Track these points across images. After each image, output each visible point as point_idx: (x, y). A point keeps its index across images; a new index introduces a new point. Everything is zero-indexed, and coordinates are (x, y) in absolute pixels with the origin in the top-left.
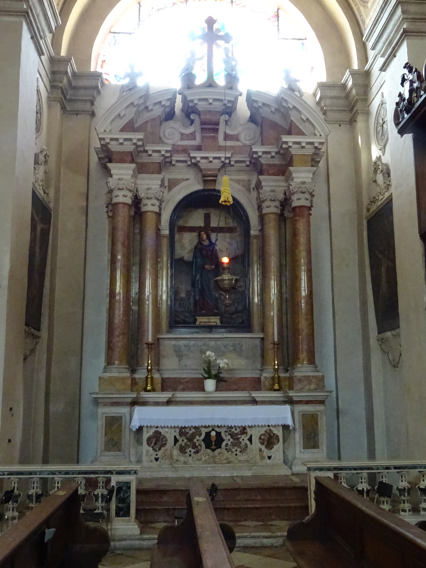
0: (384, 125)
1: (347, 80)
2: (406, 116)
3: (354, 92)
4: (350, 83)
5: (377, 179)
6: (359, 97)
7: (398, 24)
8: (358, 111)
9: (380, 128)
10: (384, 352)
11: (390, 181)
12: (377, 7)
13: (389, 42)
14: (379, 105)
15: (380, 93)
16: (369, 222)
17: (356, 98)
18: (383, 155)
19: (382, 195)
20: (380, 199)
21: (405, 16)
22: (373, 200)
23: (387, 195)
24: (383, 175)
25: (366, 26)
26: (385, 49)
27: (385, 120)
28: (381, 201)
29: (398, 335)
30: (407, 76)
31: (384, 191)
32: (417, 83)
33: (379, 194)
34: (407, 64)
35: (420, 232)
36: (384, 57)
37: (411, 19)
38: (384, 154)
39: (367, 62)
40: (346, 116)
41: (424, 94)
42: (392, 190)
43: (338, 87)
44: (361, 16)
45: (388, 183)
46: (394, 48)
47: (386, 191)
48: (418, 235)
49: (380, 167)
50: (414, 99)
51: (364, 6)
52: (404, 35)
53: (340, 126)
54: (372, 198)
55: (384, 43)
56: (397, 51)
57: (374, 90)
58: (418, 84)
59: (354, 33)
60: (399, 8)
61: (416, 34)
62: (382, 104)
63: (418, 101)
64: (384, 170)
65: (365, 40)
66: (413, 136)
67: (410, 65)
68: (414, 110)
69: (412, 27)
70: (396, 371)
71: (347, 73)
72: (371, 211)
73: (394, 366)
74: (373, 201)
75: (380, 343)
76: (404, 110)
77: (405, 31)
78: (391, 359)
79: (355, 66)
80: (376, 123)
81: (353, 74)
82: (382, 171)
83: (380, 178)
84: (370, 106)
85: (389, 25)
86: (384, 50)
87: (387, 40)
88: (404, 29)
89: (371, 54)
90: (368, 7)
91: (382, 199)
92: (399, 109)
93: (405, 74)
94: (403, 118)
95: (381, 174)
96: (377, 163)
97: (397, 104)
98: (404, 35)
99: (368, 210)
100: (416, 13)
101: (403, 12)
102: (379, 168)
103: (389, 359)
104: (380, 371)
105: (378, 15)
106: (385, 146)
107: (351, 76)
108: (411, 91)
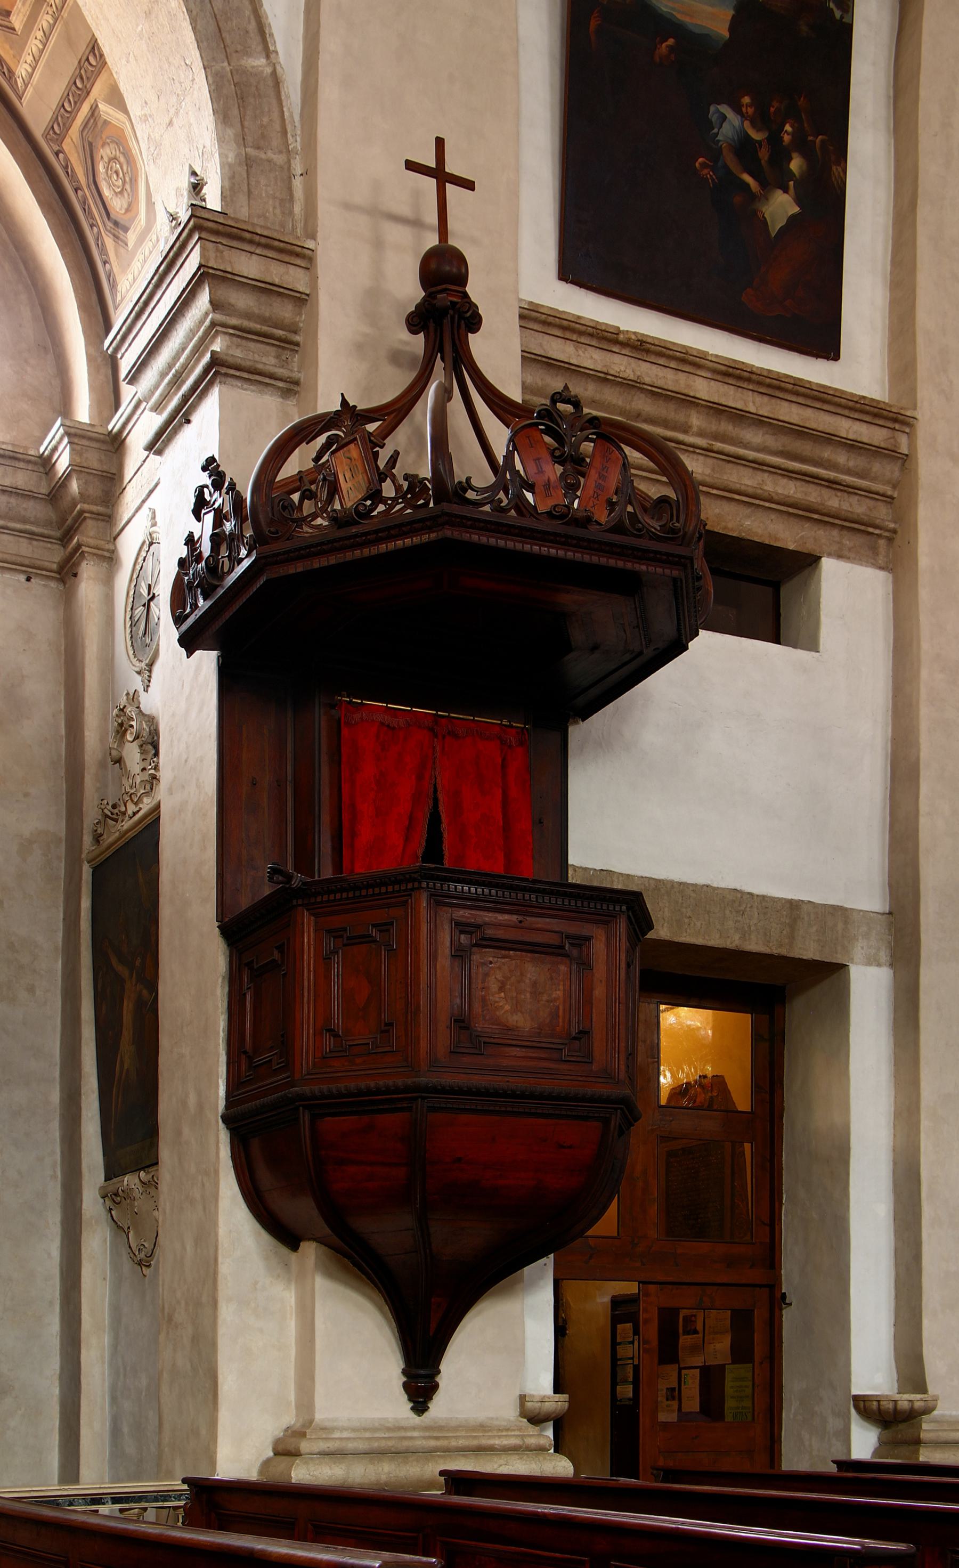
0: (152, 603)
1: (55, 449)
2: (201, 602)
3: (74, 486)
4: (63, 463)
5: (124, 754)
6: (86, 507)
7: (200, 333)
8: (84, 548)
9: (140, 610)
10: (119, 1227)
11: (156, 768)
12: (151, 252)
13: (174, 376)
14: (144, 543)
15: (145, 512)
16: (96, 871)
17: (79, 507)
18: (146, 690)
19: (136, 804)
20: (130, 812)
21: (219, 317)
22: (112, 814)
23: (147, 804)
24: (141, 746)
25: (119, 298)
26: (164, 390)
27: (156, 591)
28: (131, 818)
29: (151, 1185)
30: (211, 495)
31: (142, 791)
32: (233, 523)
33: (127, 798)
34: (211, 460)
35: (220, 916)
36: (160, 413)
37: (234, 328)
38: (148, 686)
39: (117, 405)
40: (53, 555)
41: (246, 557)
42: (162, 792)
43: (29, 462)
44: (105, 263)
45: (152, 772)
46: (185, 398)
47: (147, 794)
48: (217, 924)
49: (134, 723)
50: (223, 562)
51: (116, 237)
52: (214, 370)
53: (28, 579)
54: (109, 807)
55: (163, 375)
56: (194, 407)
57: (131, 497)
58: (235, 526)
59: (83, 307)
60: (204, 289)
61: (245, 375)
62: (151, 544)
63: (231, 570)
64: (145, 734)
65: (111, 349)
66: (219, 657)
67: (218, 466)
68: (221, 592)
69: (238, 353)
70: (145, 1276)
71: (57, 430)
72: (108, 839)
73: (140, 1263)
74: (113, 814)
75: (109, 1203)
76: (198, 586)
77: (216, 361)
78: (133, 1245)
79: (83, 412)
80: (132, 593)
81: (75, 434)
82: (137, 738)
83: (132, 754)
84: (117, 540)
85: (178, 326)
86: (161, 395)
87: (170, 366)
88: (213, 353)
89: (128, 393)
90: (127, 245)
91: (135, 814)
92: (186, 578)
93: (207, 487)
94: (195, 606)
95: (135, 742)
96: (128, 710)
97: (182, 563)
98: (214, 370)
99: (97, 838)
100: (248, 316)
101: (215, 305)
102: (132, 726)
103: (130, 1247)
104: (105, 1279)
105: (148, 291)
106: (151, 665)
107: (66, 440)
108: (216, 539)
